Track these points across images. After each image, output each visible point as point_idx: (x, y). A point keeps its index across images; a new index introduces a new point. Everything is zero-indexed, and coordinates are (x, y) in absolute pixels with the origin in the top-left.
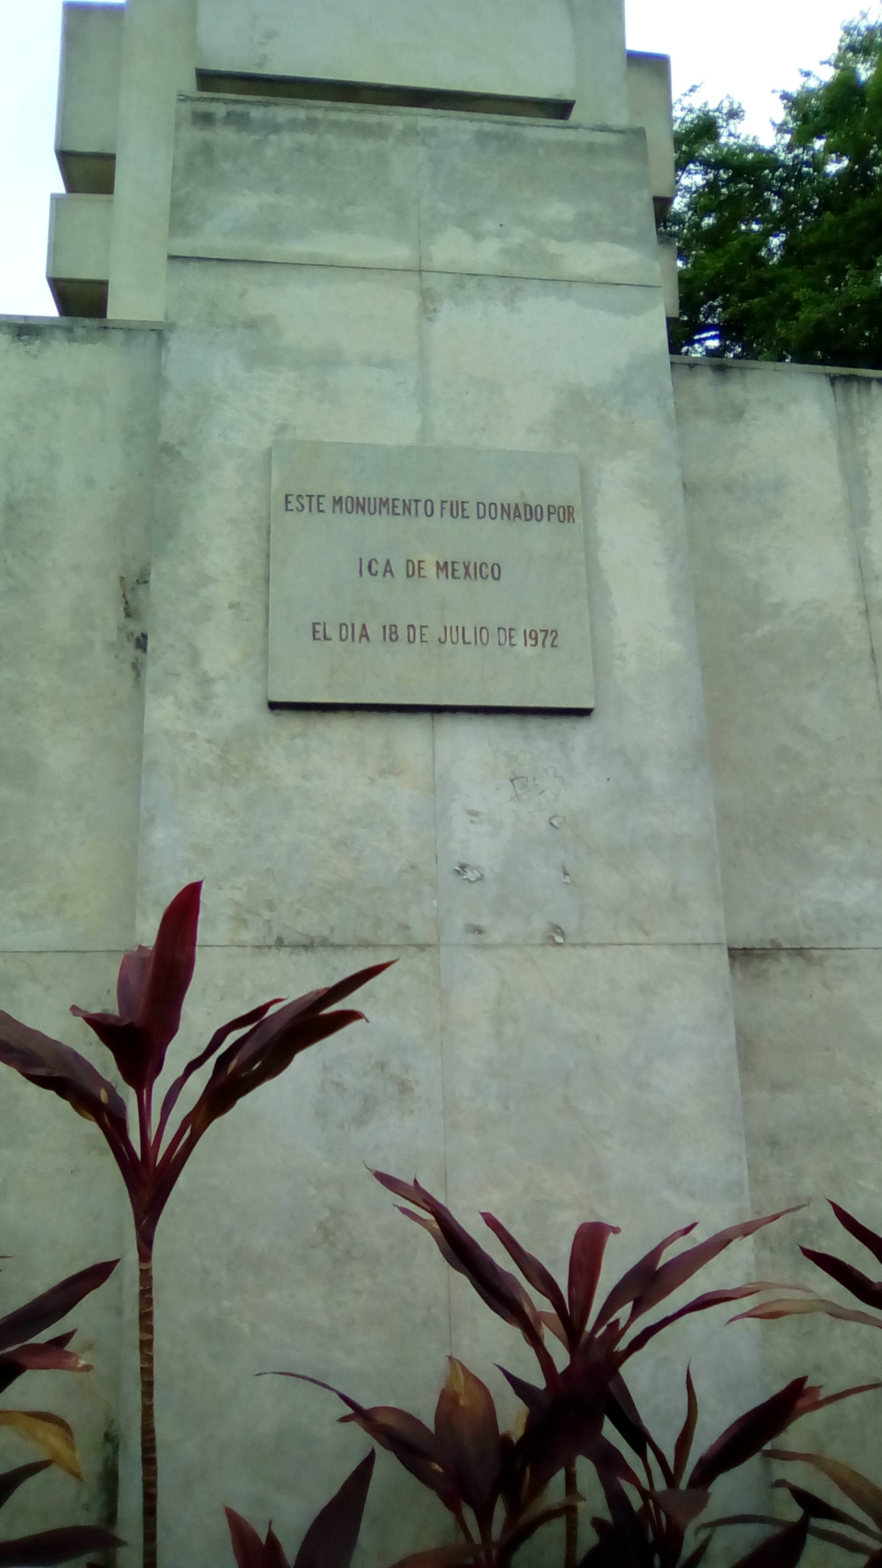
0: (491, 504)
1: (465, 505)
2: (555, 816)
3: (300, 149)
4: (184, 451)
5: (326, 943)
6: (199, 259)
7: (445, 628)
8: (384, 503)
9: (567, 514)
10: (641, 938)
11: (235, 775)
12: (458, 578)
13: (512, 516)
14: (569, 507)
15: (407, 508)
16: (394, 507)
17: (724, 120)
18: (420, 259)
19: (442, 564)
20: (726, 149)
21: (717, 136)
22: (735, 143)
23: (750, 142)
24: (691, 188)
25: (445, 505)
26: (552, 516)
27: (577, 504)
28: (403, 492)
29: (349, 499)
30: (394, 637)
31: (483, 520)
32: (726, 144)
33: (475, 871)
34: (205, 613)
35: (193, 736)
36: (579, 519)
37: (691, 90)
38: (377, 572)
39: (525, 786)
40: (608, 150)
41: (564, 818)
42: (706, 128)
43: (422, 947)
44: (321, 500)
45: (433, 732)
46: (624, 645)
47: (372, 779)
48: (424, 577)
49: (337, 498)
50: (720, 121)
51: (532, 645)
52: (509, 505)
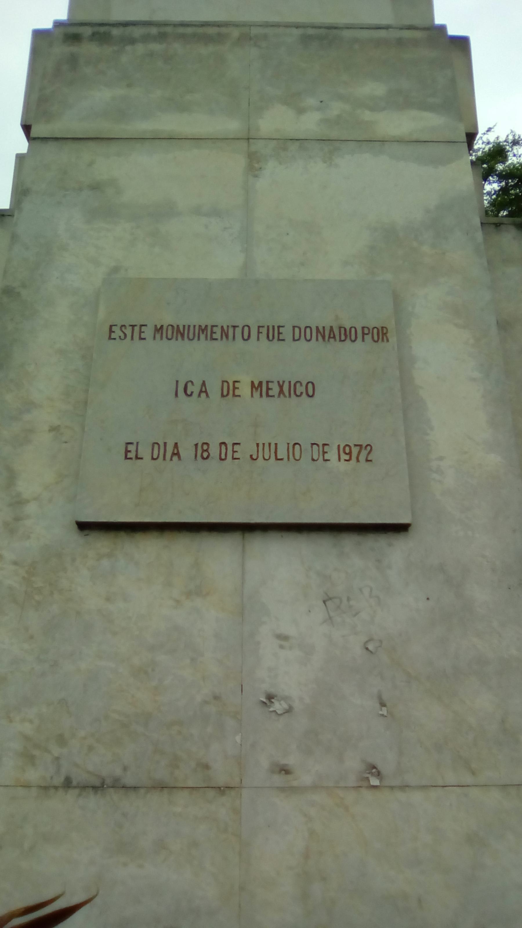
0: (306, 327)
1: (281, 330)
2: (371, 640)
3: (151, 54)
5: (117, 785)
6: (56, 139)
7: (258, 445)
8: (203, 329)
9: (381, 334)
10: (468, 779)
11: (37, 598)
13: (327, 338)
14: (382, 328)
16: (212, 332)
18: (249, 130)
20: (512, 167)
22: (518, 163)
24: (491, 192)
25: (261, 330)
26: (365, 336)
27: (391, 325)
29: (170, 328)
31: (297, 342)
32: (512, 163)
33: (282, 702)
36: (393, 339)
37: (488, 131)
38: (192, 392)
39: (339, 607)
40: (415, 43)
41: (381, 641)
42: (498, 152)
43: (222, 790)
44: (143, 329)
45: (244, 551)
46: (441, 458)
47: (178, 602)
49: (159, 327)
50: (508, 147)
51: (346, 460)
52: (324, 327)
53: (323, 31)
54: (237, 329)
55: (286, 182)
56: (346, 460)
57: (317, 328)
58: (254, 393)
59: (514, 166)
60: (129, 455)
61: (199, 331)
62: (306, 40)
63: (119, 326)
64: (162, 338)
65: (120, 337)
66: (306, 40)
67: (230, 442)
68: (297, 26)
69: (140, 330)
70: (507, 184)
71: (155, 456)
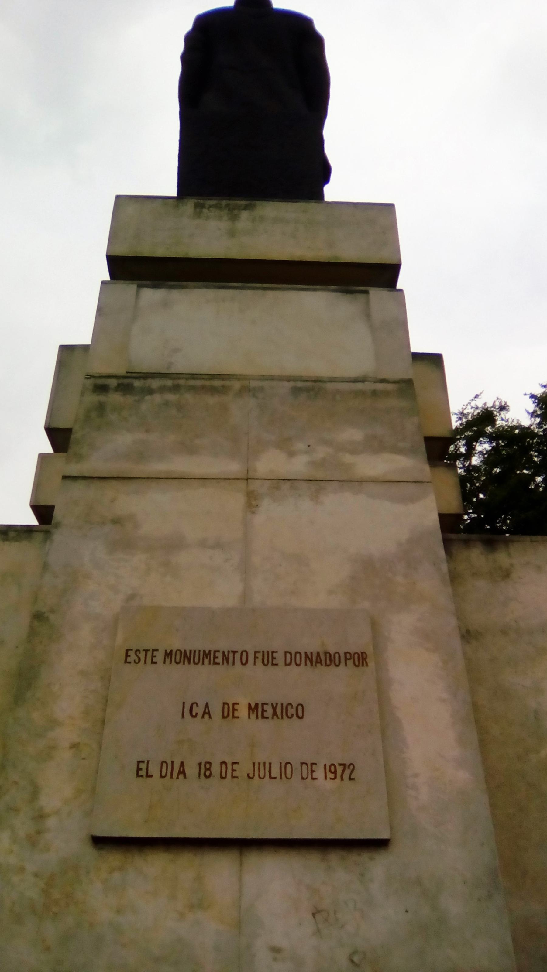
3: (167, 403)
4: (52, 617)
6: (85, 478)
7: (254, 764)
8: (207, 654)
9: (360, 659)
12: (267, 718)
14: (362, 653)
15: (226, 658)
16: (215, 657)
17: (498, 412)
19: (253, 706)
20: (501, 429)
21: (495, 421)
22: (506, 425)
23: (515, 423)
25: (257, 655)
26: (348, 661)
27: (370, 651)
28: (223, 645)
29: (178, 652)
30: (208, 773)
32: (501, 426)
34: (48, 753)
35: (22, 870)
37: (475, 397)
38: (197, 714)
39: (326, 920)
42: (486, 417)
44: (155, 653)
45: (241, 864)
46: (416, 775)
48: (238, 717)
49: (168, 651)
50: (495, 413)
51: (331, 779)
52: (312, 653)
53: (309, 384)
54: (236, 654)
55: (279, 517)
56: (331, 779)
57: (306, 653)
58: (251, 715)
59: (503, 428)
60: (141, 773)
61: (203, 657)
62: (296, 391)
63: (134, 651)
64: (171, 662)
65: (135, 660)
66: (296, 391)
67: (229, 761)
68: (289, 379)
69: (153, 653)
70: (498, 444)
71: (163, 774)
